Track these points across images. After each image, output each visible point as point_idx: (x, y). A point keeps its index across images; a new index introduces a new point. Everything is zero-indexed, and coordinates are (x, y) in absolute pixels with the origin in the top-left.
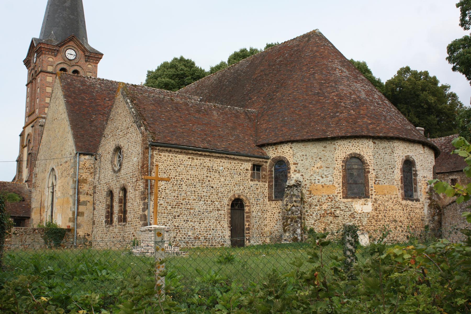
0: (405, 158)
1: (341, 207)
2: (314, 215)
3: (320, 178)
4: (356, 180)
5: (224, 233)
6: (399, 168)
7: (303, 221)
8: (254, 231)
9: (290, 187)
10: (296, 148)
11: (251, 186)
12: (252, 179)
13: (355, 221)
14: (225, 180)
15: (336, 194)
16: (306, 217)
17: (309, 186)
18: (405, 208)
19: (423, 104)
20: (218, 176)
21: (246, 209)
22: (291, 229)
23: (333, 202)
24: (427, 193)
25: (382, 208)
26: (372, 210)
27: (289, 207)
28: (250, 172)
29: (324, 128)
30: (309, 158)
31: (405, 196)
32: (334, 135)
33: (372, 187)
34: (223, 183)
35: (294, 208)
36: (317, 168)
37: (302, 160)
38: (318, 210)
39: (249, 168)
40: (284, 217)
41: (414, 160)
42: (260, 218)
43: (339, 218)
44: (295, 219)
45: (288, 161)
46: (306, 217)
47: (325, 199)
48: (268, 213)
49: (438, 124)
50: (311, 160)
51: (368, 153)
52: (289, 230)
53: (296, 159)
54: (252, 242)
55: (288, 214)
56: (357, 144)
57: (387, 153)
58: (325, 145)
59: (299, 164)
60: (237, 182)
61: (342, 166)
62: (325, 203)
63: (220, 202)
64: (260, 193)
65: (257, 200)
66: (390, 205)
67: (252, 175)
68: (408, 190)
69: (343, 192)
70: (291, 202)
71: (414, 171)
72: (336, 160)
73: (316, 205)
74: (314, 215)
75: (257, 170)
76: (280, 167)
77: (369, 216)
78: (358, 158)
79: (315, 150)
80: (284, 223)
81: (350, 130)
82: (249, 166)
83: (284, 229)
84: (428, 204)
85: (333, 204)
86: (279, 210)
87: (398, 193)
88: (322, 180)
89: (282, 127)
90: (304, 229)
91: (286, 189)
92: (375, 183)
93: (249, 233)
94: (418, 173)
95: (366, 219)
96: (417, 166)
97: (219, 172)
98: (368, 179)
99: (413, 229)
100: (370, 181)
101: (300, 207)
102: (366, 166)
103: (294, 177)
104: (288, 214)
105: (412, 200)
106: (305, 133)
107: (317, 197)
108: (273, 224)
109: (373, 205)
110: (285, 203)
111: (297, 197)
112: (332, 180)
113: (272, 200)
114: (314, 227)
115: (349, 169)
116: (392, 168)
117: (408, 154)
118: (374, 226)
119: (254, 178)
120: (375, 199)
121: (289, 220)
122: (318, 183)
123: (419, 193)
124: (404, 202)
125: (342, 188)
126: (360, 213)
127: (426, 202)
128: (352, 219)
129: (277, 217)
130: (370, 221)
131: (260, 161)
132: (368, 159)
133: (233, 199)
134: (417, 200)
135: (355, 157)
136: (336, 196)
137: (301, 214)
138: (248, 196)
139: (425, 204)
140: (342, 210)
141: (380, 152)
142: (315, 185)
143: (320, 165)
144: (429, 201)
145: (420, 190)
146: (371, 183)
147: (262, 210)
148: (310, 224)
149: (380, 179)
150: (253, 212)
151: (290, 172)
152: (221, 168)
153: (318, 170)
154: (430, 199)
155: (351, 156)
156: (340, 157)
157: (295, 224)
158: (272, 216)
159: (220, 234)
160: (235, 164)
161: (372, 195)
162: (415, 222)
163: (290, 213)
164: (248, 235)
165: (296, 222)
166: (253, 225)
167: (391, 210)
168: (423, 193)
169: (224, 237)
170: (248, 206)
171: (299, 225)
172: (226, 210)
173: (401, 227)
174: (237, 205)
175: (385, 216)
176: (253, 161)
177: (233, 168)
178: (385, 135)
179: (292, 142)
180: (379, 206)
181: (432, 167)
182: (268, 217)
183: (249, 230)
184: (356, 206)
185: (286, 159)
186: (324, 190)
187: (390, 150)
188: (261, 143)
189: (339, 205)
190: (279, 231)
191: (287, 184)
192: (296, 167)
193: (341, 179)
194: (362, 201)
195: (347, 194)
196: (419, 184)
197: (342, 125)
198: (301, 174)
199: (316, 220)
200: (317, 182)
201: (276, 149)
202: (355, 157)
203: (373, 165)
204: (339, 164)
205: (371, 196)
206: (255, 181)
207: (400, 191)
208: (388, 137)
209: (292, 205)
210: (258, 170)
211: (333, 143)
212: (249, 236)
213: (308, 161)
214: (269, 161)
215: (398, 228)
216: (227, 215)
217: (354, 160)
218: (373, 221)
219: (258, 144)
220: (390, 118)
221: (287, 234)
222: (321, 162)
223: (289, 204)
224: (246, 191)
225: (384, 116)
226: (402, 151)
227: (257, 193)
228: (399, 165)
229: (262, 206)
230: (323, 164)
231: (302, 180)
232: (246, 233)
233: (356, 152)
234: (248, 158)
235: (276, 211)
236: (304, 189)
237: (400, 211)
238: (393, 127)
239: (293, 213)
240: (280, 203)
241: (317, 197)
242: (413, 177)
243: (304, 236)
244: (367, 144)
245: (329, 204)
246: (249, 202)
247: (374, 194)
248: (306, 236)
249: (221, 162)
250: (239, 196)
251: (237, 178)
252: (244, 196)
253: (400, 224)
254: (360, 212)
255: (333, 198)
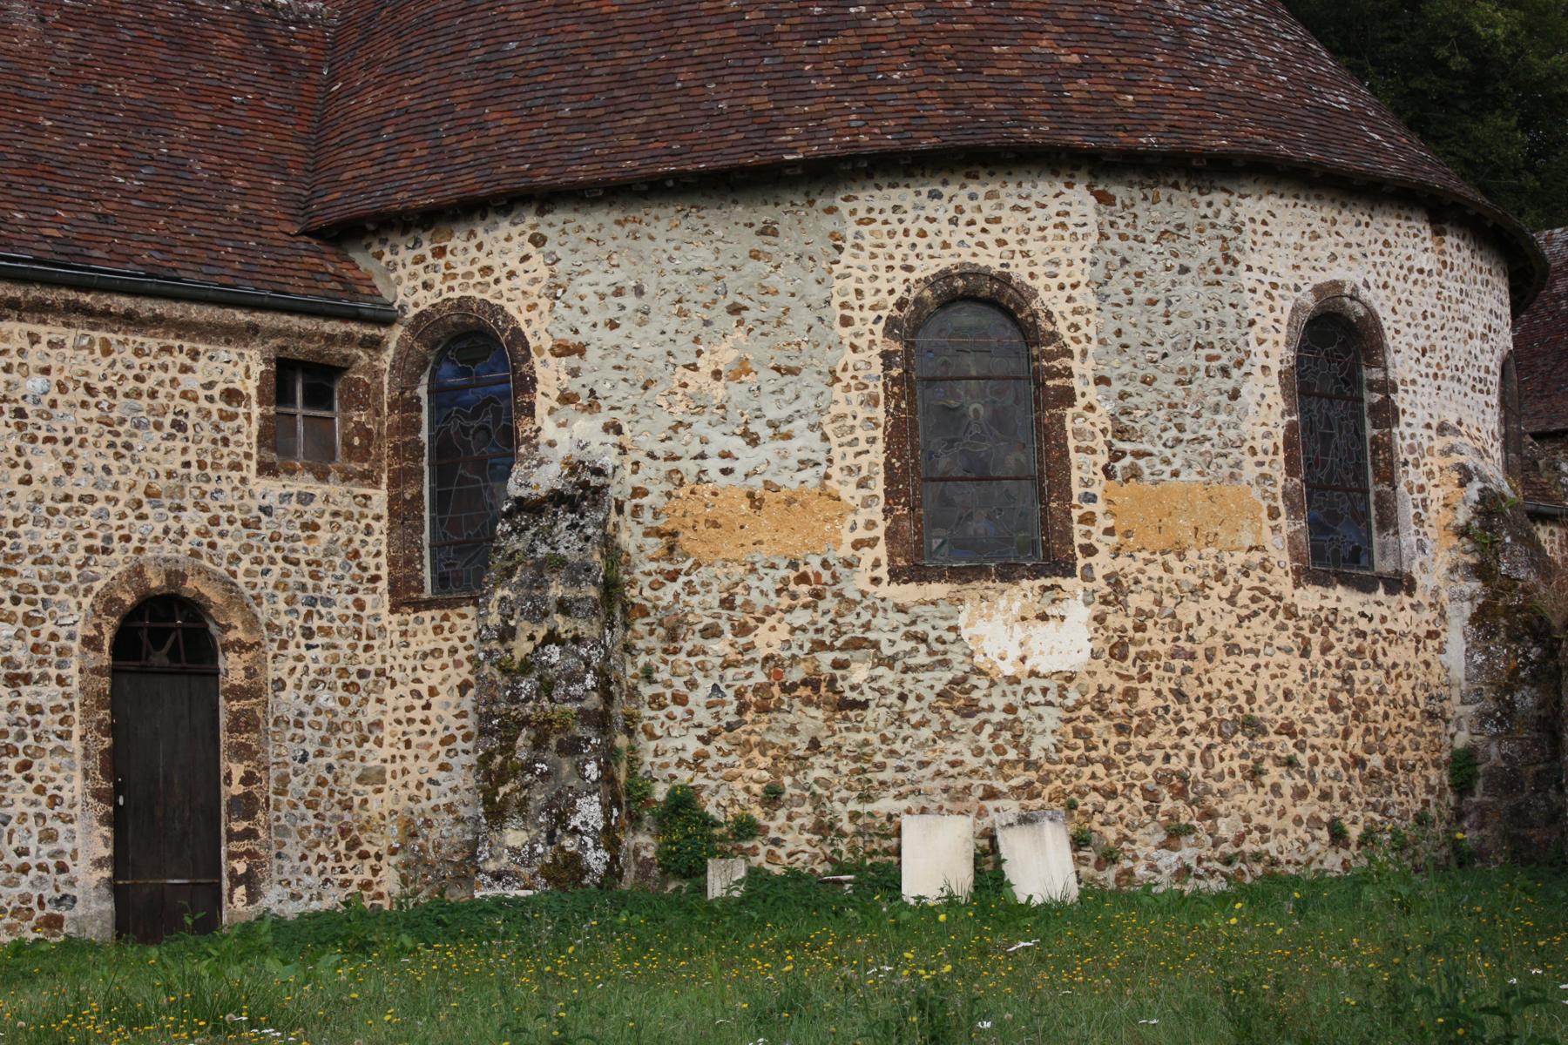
0: (1310, 301)
1: (883, 639)
2: (698, 697)
3: (737, 444)
4: (979, 456)
5: (63, 844)
6: (1276, 367)
7: (621, 741)
8: (285, 811)
9: (530, 507)
10: (573, 239)
11: (267, 510)
12: (272, 457)
13: (978, 730)
14: (68, 467)
15: (846, 551)
16: (646, 712)
17: (661, 503)
18: (1316, 639)
19: (1442, 52)
20: (15, 441)
21: (232, 668)
22: (540, 797)
23: (829, 603)
24: (1463, 532)
25: (1157, 639)
26: (1095, 655)
27: (521, 647)
28: (256, 411)
29: (760, 102)
30: (662, 310)
31: (1317, 553)
32: (831, 144)
33: (1092, 499)
34: (48, 491)
35: (554, 653)
36: (717, 375)
37: (613, 325)
38: (727, 665)
39: (251, 387)
40: (488, 717)
41: (1372, 314)
42: (334, 728)
43: (869, 715)
44: (565, 727)
45: (518, 334)
46: (646, 712)
47: (769, 585)
48: (389, 694)
49: (1531, 168)
50: (675, 323)
51: (1063, 270)
52: (523, 804)
53: (573, 317)
54: (273, 898)
55: (514, 698)
56: (988, 208)
57: (1194, 265)
58: (765, 214)
59: (592, 354)
60: (161, 484)
61: (886, 356)
62: (769, 612)
63: (28, 619)
64: (328, 552)
65: (312, 602)
66: (1212, 616)
67: (274, 437)
68: (1335, 517)
69: (891, 535)
70: (538, 614)
71: (1372, 386)
72: (846, 322)
73: (711, 632)
74: (698, 697)
75: (308, 402)
76: (465, 372)
77: (1073, 696)
78: (992, 302)
79: (701, 254)
80: (490, 755)
81: (938, 112)
82: (244, 367)
83: (488, 800)
84: (1467, 609)
85: (823, 621)
86: (465, 672)
87: (1267, 537)
88: (747, 458)
89: (479, 102)
90: (626, 799)
91: (503, 527)
92: (1108, 472)
93: (250, 834)
94: (1401, 400)
95: (1052, 717)
96: (1391, 358)
97: (20, 413)
98: (1063, 448)
99: (1374, 775)
100: (1074, 457)
101: (598, 642)
102: (1051, 356)
103: (558, 439)
104: (514, 698)
105: (1366, 586)
106: (632, 140)
107: (716, 576)
108: (421, 767)
109: (1100, 619)
110: (495, 619)
111: (577, 573)
112: (821, 457)
113: (419, 605)
114: (700, 780)
115: (931, 381)
116: (1225, 371)
117: (1336, 273)
118: (1108, 763)
119: (289, 452)
120: (1113, 580)
121: (523, 739)
122: (723, 481)
123: (1408, 539)
124: (1309, 598)
125: (887, 512)
126: (1013, 680)
127: (1457, 598)
128: (957, 722)
129: (448, 716)
130: (1077, 733)
131: (330, 339)
132: (1059, 306)
133: (129, 599)
134: (1400, 583)
135: (969, 298)
136: (849, 564)
137: (608, 698)
138: (241, 580)
139: (1450, 609)
140: (890, 662)
141: (1145, 261)
142: (705, 490)
143: (734, 354)
144: (1476, 585)
145: (1418, 518)
146: (1084, 469)
147: (343, 672)
148: (672, 758)
149: (1145, 446)
150: (280, 685)
151: (530, 411)
152: (36, 383)
153: (719, 391)
154: (1482, 571)
155: (942, 287)
156: (869, 300)
157: (566, 766)
158: (418, 714)
159: (33, 844)
160: (138, 352)
161: (1089, 550)
162: (1384, 727)
163: (527, 685)
164: (244, 846)
165: (571, 747)
166: (284, 780)
167: (1221, 655)
168: (1433, 533)
169: (62, 868)
170: (241, 647)
171: (592, 770)
172: (70, 684)
173: (1290, 763)
174: (163, 644)
175: (1179, 695)
176: (276, 333)
177: (130, 385)
178: (1171, 143)
179: (546, 199)
180: (1140, 628)
181: (1495, 366)
182: (387, 720)
183: (249, 815)
184: (981, 627)
185: (508, 318)
186: (764, 524)
187: (1212, 249)
188: (334, 215)
189: (867, 627)
190: (464, 812)
191: (513, 489)
192: (574, 373)
193: (880, 445)
194: (1023, 594)
195: (919, 550)
196: (1411, 476)
197: (887, 81)
198: (605, 416)
199: (714, 734)
200: (713, 473)
201: (440, 252)
202: (969, 298)
203: (1093, 347)
204: (862, 343)
205: (1081, 562)
206: (291, 472)
207: (1282, 520)
208: (1199, 155)
209: (541, 633)
210: (319, 397)
211: (822, 202)
212: (250, 854)
213: (652, 329)
214: (395, 335)
215: (1273, 774)
216: (86, 713)
217: (965, 317)
218: (1099, 728)
219: (317, 222)
220: (1214, 37)
221: (514, 836)
222: (740, 334)
223: (525, 628)
224: (228, 545)
225: (1170, 20)
226: (1291, 250)
227: (306, 563)
228: (1274, 350)
229: (344, 643)
230: (760, 351)
231: (609, 459)
232: (232, 836)
233: (982, 261)
234: (241, 316)
235: (445, 677)
236: (626, 521)
237: (1281, 657)
238: (1233, 94)
239: (546, 687)
240: (465, 622)
241: (716, 576)
242: (1370, 432)
243: (630, 840)
244: (1054, 206)
245: (801, 617)
246: (252, 623)
247: (1104, 545)
248: (644, 843)
249: (34, 339)
250: (175, 577)
251: (157, 454)
252: (211, 577)
253: (1285, 746)
254: (1008, 669)
255: (826, 576)
